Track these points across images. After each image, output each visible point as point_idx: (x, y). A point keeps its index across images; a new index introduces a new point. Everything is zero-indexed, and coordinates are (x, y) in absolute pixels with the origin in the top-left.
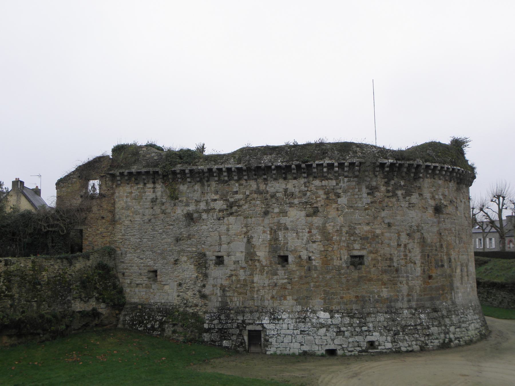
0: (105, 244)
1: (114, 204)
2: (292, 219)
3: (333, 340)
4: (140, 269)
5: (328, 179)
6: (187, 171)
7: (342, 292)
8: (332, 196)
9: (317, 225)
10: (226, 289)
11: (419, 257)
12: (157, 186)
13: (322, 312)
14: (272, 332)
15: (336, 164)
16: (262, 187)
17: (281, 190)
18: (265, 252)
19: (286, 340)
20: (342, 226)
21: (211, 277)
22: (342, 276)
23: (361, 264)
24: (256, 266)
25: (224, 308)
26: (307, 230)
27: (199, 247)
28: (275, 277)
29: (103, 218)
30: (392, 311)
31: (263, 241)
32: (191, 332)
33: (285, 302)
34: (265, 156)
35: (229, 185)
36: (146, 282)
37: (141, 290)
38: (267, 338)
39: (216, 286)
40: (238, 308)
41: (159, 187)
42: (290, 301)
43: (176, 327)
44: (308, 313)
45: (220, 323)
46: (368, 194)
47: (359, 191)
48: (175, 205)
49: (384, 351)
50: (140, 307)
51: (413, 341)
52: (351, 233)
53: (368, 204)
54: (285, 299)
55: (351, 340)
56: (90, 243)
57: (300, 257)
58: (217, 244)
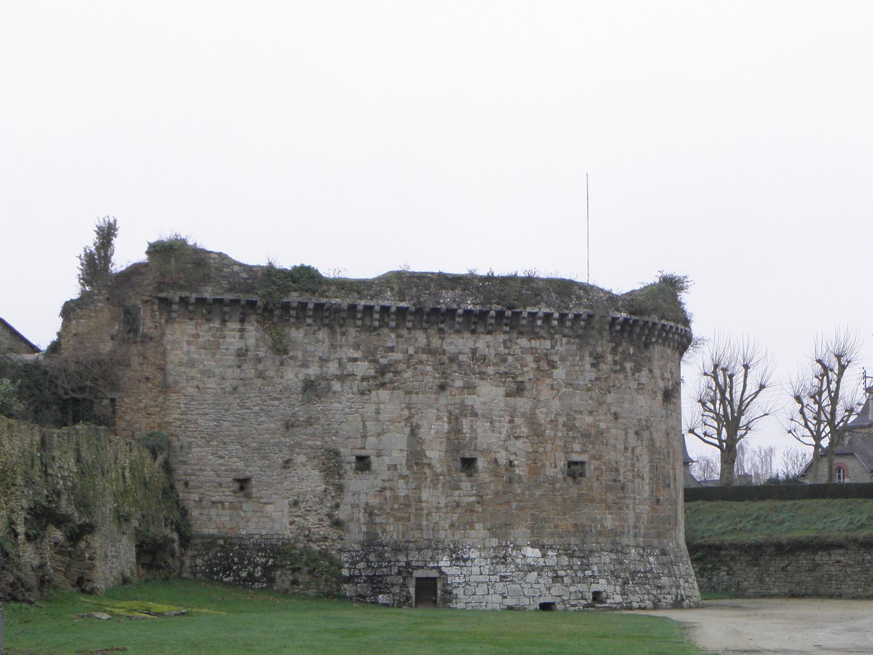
0: (151, 428)
1: (164, 354)
2: (483, 400)
3: (549, 589)
4: (218, 476)
5: (538, 337)
6: (311, 306)
7: (556, 517)
8: (544, 366)
9: (522, 410)
10: (376, 511)
11: (647, 469)
12: (248, 326)
13: (529, 548)
14: (457, 580)
15: (556, 315)
16: (436, 342)
17: (467, 350)
18: (440, 451)
19: (480, 591)
20: (557, 414)
21: (349, 491)
22: (557, 493)
23: (582, 475)
24: (425, 474)
25: (371, 543)
26: (508, 418)
27: (327, 439)
28: (457, 493)
29: (147, 379)
30: (618, 550)
31: (437, 433)
32: (326, 580)
33: (472, 532)
34: (444, 292)
35: (379, 335)
36: (231, 499)
37: (221, 512)
38: (449, 588)
39: (357, 506)
40: (396, 542)
41: (253, 331)
42: (479, 532)
43: (297, 574)
44: (510, 550)
45: (369, 567)
46: (593, 365)
47: (580, 360)
48: (282, 364)
49: (614, 606)
50: (221, 542)
52: (570, 427)
53: (591, 381)
54: (472, 527)
55: (572, 589)
56: (127, 425)
57: (496, 461)
58: (359, 436)
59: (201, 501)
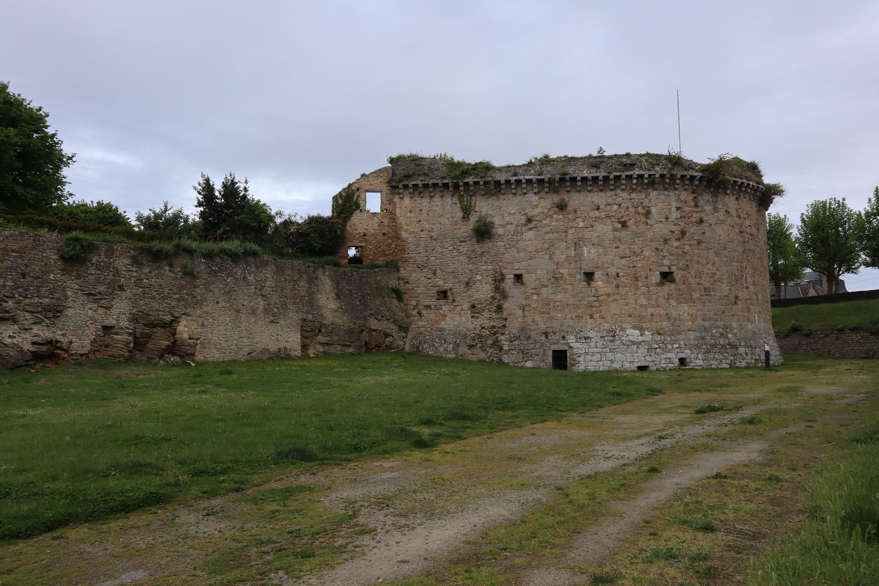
55: (662, 356)
59: (417, 305)
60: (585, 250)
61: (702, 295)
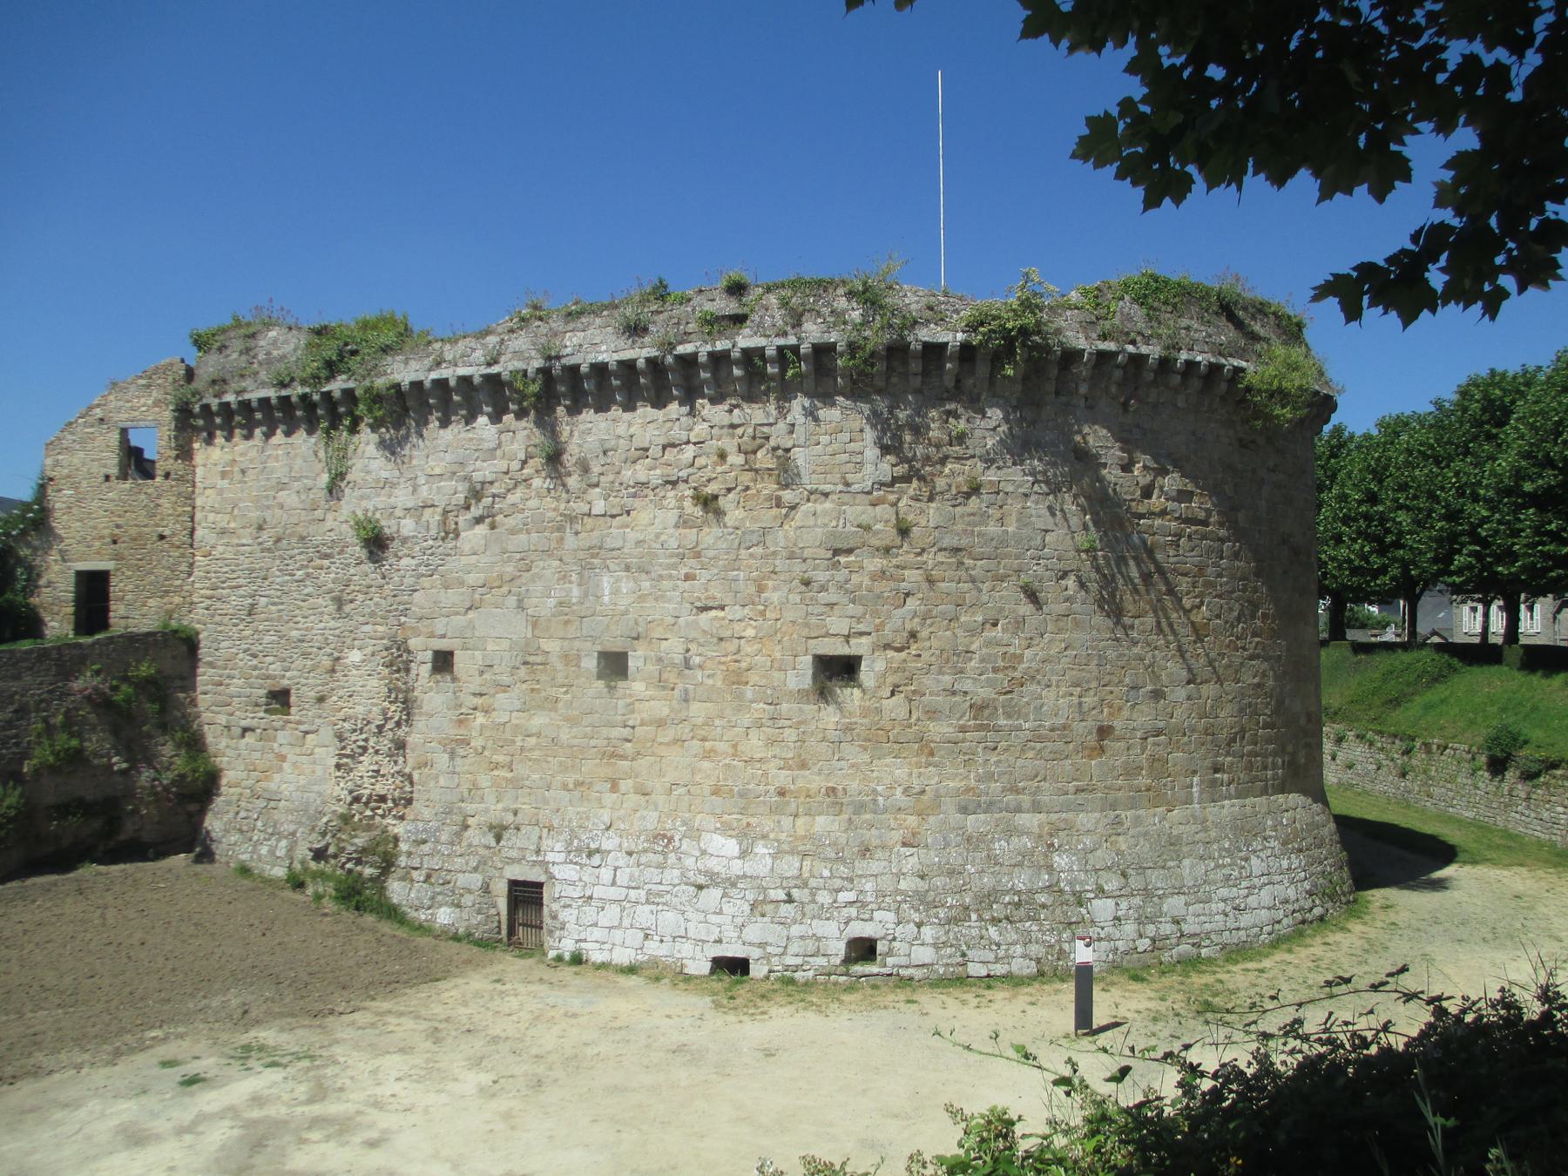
21: (421, 714)
51: (1014, 943)
55: (796, 930)
60: (606, 582)
61: (963, 729)
